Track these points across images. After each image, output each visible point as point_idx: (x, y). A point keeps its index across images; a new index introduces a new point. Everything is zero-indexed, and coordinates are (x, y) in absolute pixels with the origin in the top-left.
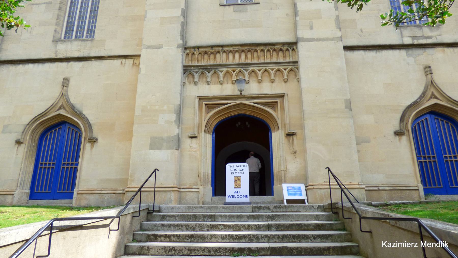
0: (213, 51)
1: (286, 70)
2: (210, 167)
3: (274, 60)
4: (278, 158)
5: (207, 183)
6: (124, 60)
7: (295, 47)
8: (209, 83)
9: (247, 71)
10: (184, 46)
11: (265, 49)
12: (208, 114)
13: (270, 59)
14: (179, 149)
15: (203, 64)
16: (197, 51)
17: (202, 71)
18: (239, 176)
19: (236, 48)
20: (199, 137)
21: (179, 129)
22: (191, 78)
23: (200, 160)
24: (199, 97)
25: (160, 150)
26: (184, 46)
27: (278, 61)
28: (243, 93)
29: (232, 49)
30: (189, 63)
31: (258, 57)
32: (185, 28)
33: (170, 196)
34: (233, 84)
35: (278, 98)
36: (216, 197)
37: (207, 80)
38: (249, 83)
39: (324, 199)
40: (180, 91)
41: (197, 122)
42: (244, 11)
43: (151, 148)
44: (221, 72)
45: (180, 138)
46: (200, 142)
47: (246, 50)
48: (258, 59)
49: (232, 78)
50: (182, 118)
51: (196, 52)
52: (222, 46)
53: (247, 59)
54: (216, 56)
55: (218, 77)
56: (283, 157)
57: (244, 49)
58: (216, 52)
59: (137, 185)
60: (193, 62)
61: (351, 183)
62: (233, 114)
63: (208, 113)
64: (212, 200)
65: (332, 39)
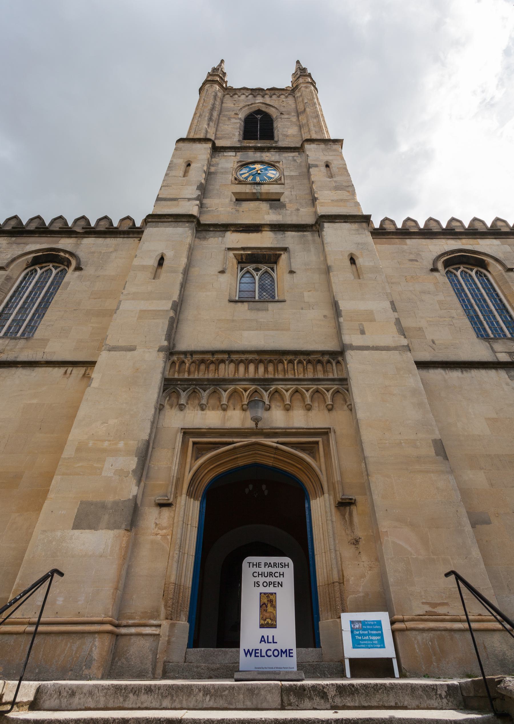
0: (214, 360)
1: (329, 391)
2: (189, 572)
3: (310, 375)
4: (325, 552)
5: (179, 611)
6: (70, 369)
7: (340, 359)
8: (204, 407)
9: (267, 391)
10: (170, 350)
11: (295, 360)
12: (198, 460)
13: (302, 374)
14: (133, 530)
15: (196, 377)
16: (189, 358)
17: (195, 388)
18: (272, 593)
19: (250, 357)
20: (174, 505)
21: (139, 486)
22: (174, 399)
23: (171, 554)
24: (184, 430)
25: (93, 531)
26: (170, 350)
27: (316, 377)
28: (260, 425)
29: (243, 357)
30: (174, 375)
31: (285, 371)
32: (175, 326)
33: (91, 648)
34: (243, 410)
35: (319, 436)
36: (196, 650)
37: (201, 403)
38: (271, 409)
39: (434, 658)
40: (153, 417)
41: (175, 475)
42: (263, 310)
43: (77, 526)
44: (225, 391)
45: (139, 505)
46: (176, 515)
47: (266, 360)
48: (285, 373)
49: (242, 401)
50: (149, 466)
51: (188, 361)
52: (229, 353)
53: (268, 374)
54: (218, 367)
55: (220, 399)
56: (336, 551)
57: (263, 359)
58: (219, 361)
59: (23, 615)
60: (181, 374)
61: (480, 615)
62: (241, 463)
63: (197, 459)
64: (186, 659)
65: (395, 348)
